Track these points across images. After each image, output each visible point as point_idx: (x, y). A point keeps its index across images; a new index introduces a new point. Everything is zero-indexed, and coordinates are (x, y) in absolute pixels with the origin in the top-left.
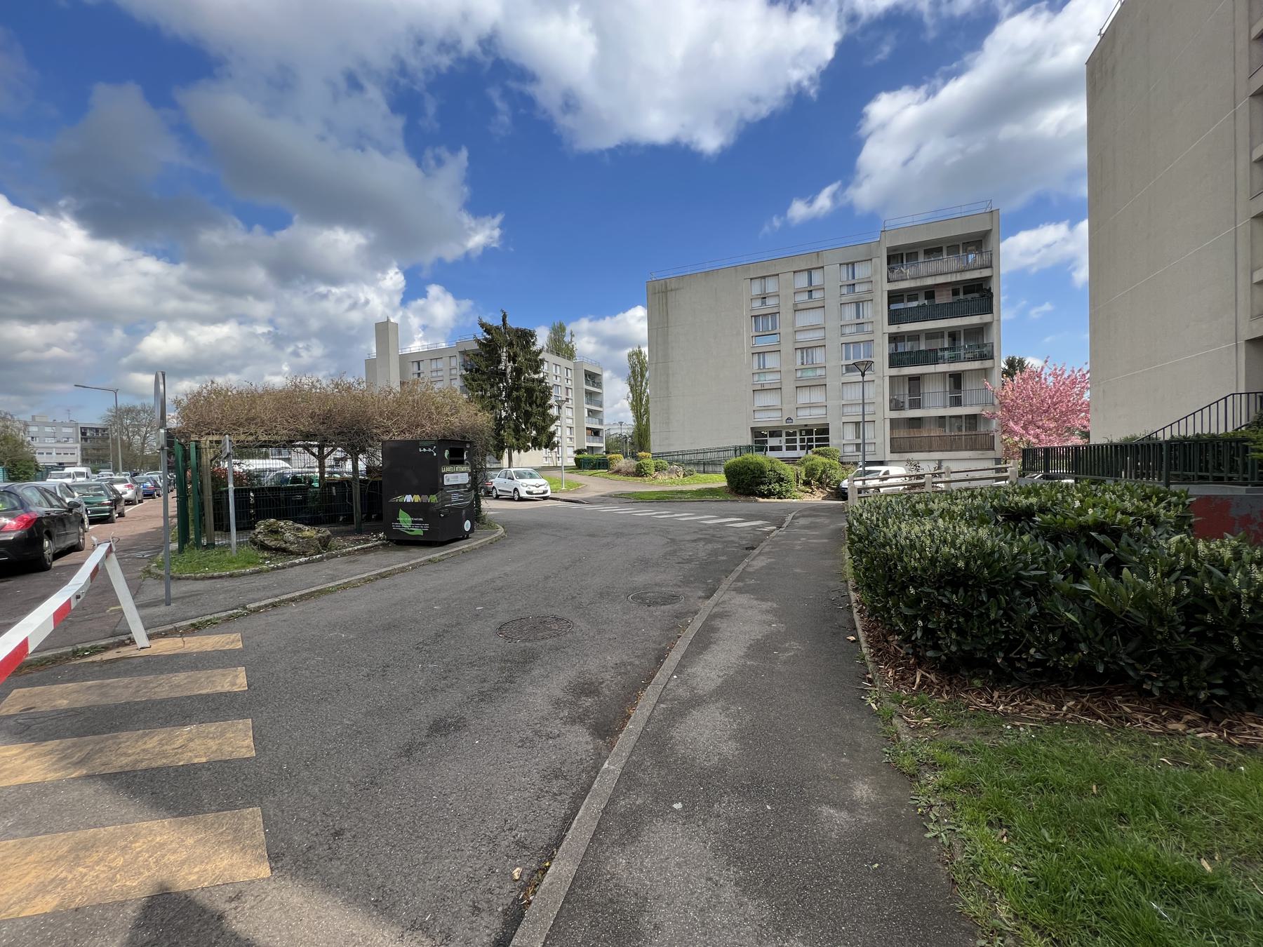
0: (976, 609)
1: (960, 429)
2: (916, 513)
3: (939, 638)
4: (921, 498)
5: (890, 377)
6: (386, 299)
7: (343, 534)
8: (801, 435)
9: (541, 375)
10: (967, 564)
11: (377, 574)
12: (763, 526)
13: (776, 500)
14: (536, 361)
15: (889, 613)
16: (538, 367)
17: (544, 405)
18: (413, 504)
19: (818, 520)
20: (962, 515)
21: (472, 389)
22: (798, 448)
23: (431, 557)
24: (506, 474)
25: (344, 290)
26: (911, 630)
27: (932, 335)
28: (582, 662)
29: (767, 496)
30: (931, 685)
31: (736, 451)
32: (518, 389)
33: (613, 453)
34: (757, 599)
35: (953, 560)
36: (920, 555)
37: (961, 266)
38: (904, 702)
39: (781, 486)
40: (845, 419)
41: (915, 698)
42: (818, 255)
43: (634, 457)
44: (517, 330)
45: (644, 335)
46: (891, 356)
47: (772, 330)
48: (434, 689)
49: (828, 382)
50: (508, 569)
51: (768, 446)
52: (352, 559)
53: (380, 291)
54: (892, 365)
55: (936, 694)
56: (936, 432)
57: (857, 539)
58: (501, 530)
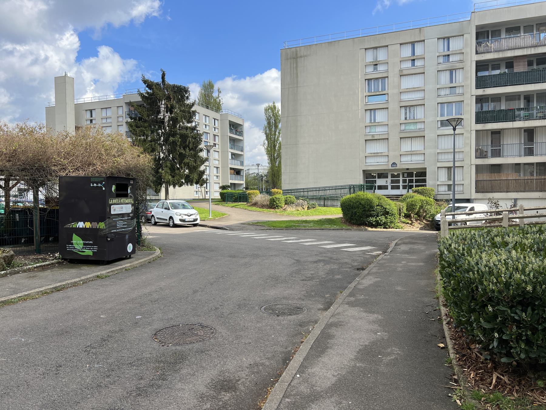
0: (540, 324)
1: (532, 174)
2: (494, 245)
3: (511, 348)
4: (498, 232)
5: (476, 131)
6: (63, 56)
7: (24, 254)
8: (403, 177)
9: (194, 124)
10: (534, 288)
11: (53, 288)
12: (371, 251)
13: (382, 230)
14: (189, 113)
15: (472, 326)
16: (191, 117)
17: (195, 149)
18: (85, 229)
19: (416, 247)
20: (531, 247)
21: (136, 134)
22: (401, 187)
23: (99, 273)
24: (163, 205)
25: (27, 48)
26: (490, 340)
27: (510, 97)
28: (222, 363)
29: (376, 226)
30: (504, 385)
31: (350, 189)
32: (174, 135)
33: (251, 189)
34: (365, 312)
35: (524, 285)
36: (497, 280)
37: (535, 42)
38: (483, 399)
39: (386, 218)
40: (439, 165)
41: (491, 396)
42: (420, 31)
43: (269, 193)
44: (174, 86)
45: (278, 93)
46: (477, 114)
47: (382, 91)
48: (99, 386)
49: (426, 134)
50: (163, 284)
51: (377, 185)
52: (32, 275)
53: (58, 50)
54: (478, 121)
55: (508, 393)
56: (512, 176)
57: (446, 265)
58: (158, 252)
